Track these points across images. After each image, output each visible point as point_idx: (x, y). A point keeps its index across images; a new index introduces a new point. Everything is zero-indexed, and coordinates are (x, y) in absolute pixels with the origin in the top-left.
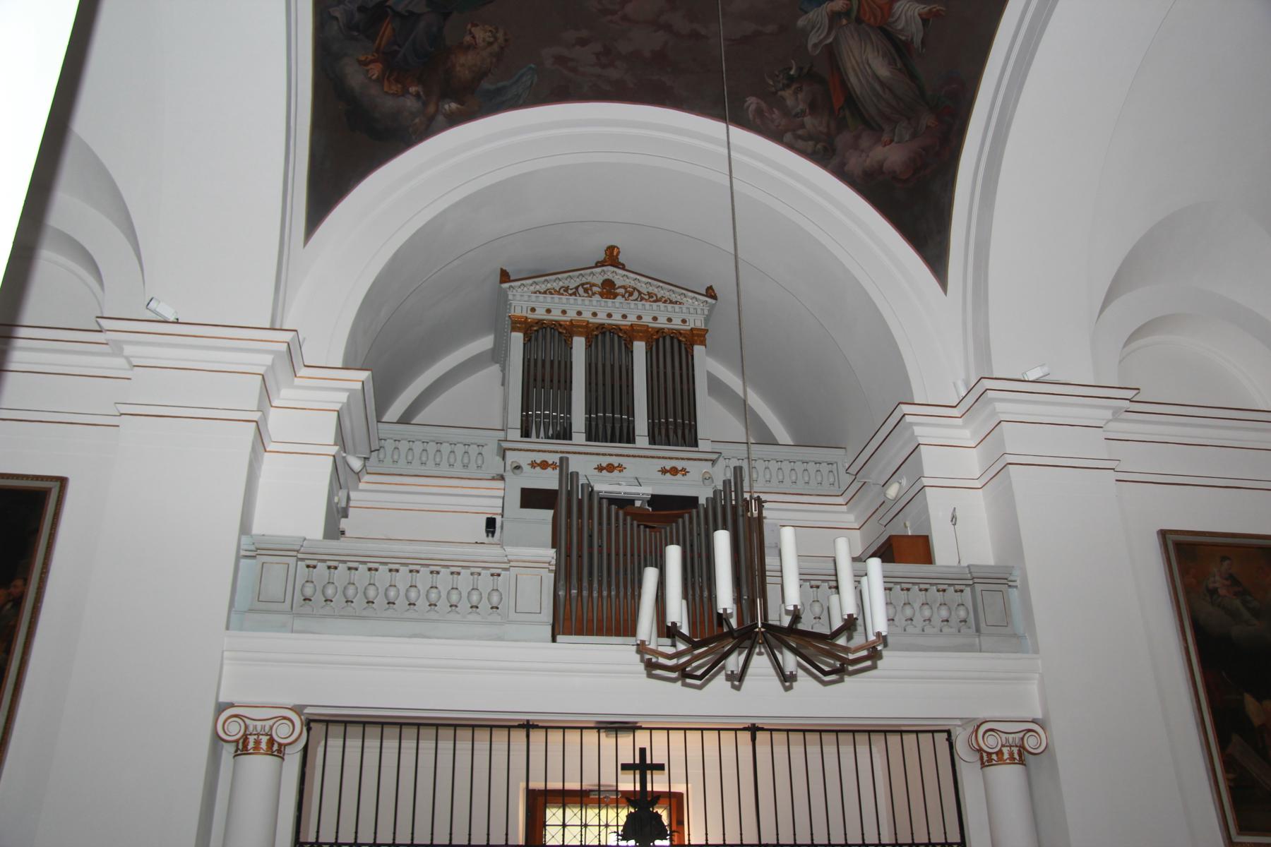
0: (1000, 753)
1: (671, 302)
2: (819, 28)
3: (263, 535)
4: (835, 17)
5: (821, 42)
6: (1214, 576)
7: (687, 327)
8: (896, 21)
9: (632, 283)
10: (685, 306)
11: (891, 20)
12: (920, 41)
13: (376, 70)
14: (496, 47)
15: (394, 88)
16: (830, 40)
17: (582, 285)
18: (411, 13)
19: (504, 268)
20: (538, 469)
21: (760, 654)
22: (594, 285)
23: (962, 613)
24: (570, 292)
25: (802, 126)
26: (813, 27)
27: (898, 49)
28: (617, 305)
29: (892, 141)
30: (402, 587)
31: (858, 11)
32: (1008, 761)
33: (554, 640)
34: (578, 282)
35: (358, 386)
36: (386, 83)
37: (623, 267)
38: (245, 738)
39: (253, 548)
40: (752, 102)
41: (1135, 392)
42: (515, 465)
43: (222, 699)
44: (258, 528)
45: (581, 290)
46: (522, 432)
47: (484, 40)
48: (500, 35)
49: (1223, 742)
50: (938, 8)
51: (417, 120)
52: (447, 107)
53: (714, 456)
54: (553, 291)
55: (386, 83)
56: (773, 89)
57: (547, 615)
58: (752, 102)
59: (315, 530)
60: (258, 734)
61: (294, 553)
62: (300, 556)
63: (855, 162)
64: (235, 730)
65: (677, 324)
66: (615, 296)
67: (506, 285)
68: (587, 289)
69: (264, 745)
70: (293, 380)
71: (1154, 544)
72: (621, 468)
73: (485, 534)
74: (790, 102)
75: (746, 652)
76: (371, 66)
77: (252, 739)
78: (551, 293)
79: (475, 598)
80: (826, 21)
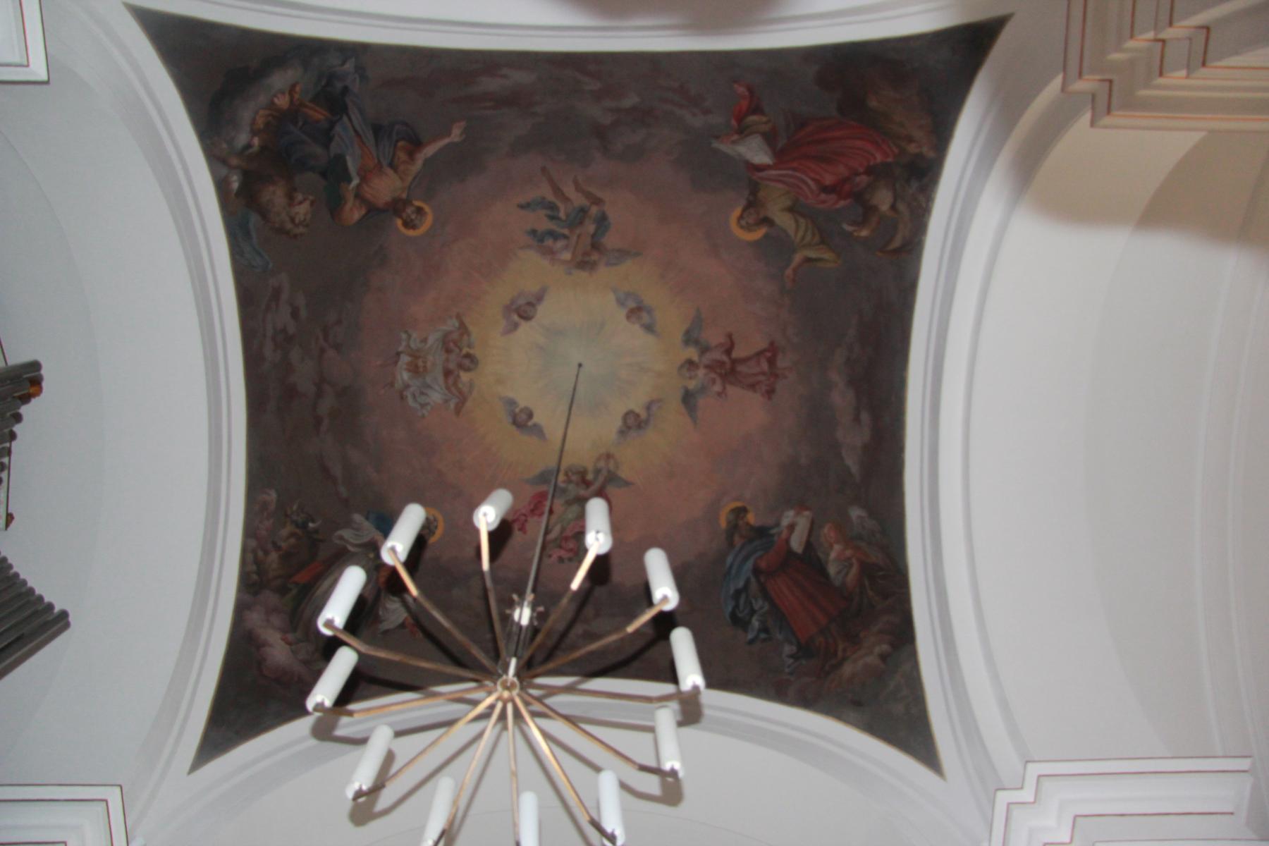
5: (347, 541)
13: (283, 102)
14: (289, 226)
16: (351, 548)
18: (330, 139)
25: (266, 553)
26: (357, 530)
29: (290, 644)
36: (267, 112)
47: (297, 213)
48: (301, 230)
51: (225, 146)
55: (267, 112)
56: (289, 512)
58: (272, 496)
63: (255, 618)
75: (716, 145)
76: (287, 98)
80: (365, 540)
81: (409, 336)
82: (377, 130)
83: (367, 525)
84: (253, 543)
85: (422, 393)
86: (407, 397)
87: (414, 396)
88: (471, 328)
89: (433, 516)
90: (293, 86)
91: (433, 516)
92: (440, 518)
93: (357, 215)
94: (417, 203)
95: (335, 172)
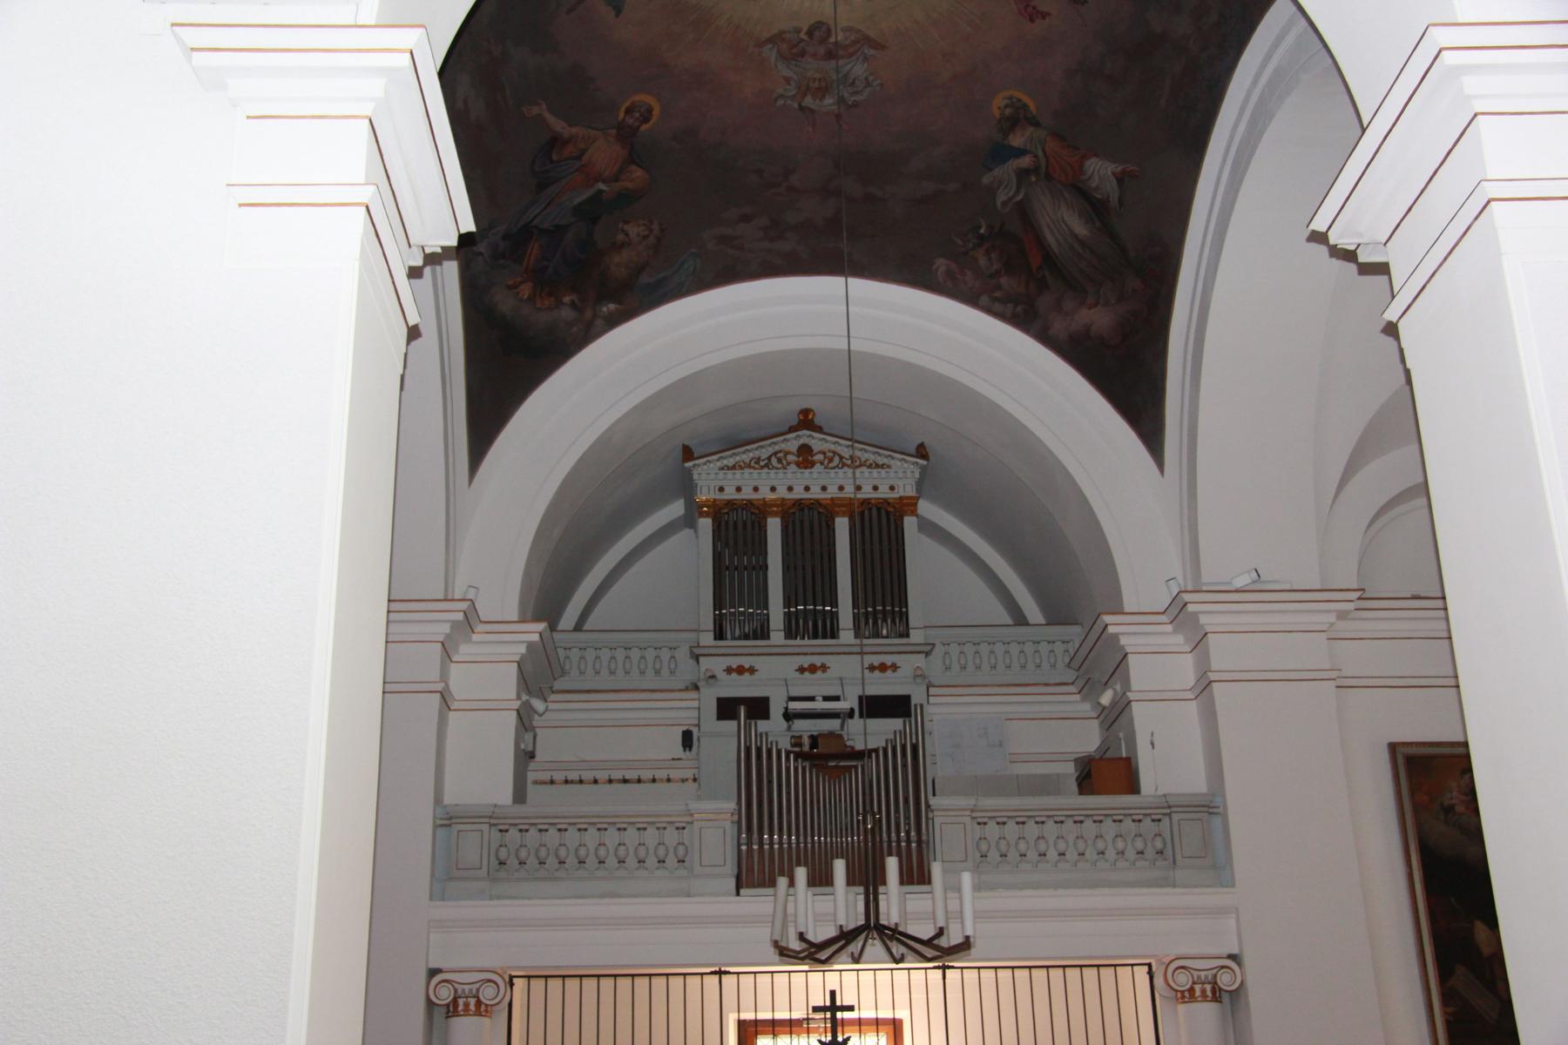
0: (1191, 990)
1: (877, 466)
2: (1007, 186)
3: (457, 805)
4: (1023, 174)
5: (1010, 199)
6: (1451, 792)
7: (895, 495)
8: (1090, 178)
9: (833, 447)
10: (891, 471)
11: (1083, 178)
12: (1117, 200)
13: (526, 290)
14: (652, 240)
15: (547, 303)
17: (775, 454)
19: (686, 443)
20: (734, 675)
21: (873, 945)
22: (787, 453)
23: (1159, 845)
24: (762, 463)
25: (999, 287)
27: (1095, 208)
28: (815, 475)
29: (1096, 305)
30: (592, 845)
31: (1047, 167)
32: (1199, 999)
33: (738, 894)
34: (771, 450)
35: (536, 637)
37: (819, 429)
38: (455, 1001)
39: (446, 816)
40: (941, 264)
41: (1362, 592)
42: (709, 674)
43: (433, 965)
44: (448, 799)
45: (774, 461)
46: (715, 634)
47: (638, 235)
48: (656, 226)
49: (1444, 973)
50: (1132, 168)
52: (605, 309)
53: (928, 648)
54: (742, 464)
57: (730, 868)
58: (941, 264)
59: (505, 796)
60: (467, 997)
61: (487, 820)
62: (492, 821)
63: (1059, 327)
64: (445, 995)
65: (884, 493)
66: (811, 464)
67: (689, 464)
68: (780, 458)
69: (472, 1007)
70: (471, 637)
71: (1384, 757)
72: (824, 668)
73: (682, 749)
74: (982, 262)
76: (522, 287)
77: (461, 1002)
78: (741, 468)
79: (661, 852)
81: (782, 96)
82: (542, 187)
83: (997, 172)
84: (984, 299)
85: (853, 83)
86: (855, 101)
87: (856, 93)
88: (775, 31)
89: (1004, 98)
90: (509, 287)
91: (1004, 98)
92: (1007, 94)
93: (638, 173)
94: (622, 115)
95: (592, 211)
